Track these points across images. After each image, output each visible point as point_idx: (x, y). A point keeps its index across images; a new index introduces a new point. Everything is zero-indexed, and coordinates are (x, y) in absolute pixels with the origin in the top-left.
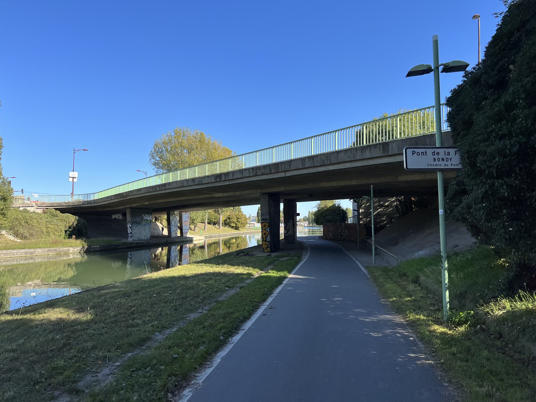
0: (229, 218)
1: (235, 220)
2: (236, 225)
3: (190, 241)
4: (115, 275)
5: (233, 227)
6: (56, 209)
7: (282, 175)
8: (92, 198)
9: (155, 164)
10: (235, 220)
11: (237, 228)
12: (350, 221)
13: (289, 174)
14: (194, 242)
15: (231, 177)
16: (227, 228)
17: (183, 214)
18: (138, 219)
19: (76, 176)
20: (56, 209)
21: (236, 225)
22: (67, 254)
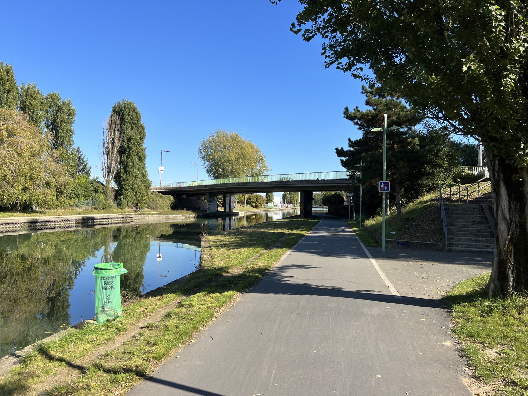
0: (250, 199)
1: (255, 200)
2: (256, 204)
3: (237, 214)
4: (80, 256)
5: (253, 206)
6: (159, 192)
7: (315, 185)
8: (182, 185)
9: (203, 158)
10: (255, 200)
11: (256, 207)
12: (346, 204)
13: (317, 185)
14: (240, 216)
15: (288, 183)
16: (249, 207)
17: (232, 197)
18: (212, 199)
19: (163, 169)
20: (159, 192)
21: (256, 204)
22: (189, 218)
